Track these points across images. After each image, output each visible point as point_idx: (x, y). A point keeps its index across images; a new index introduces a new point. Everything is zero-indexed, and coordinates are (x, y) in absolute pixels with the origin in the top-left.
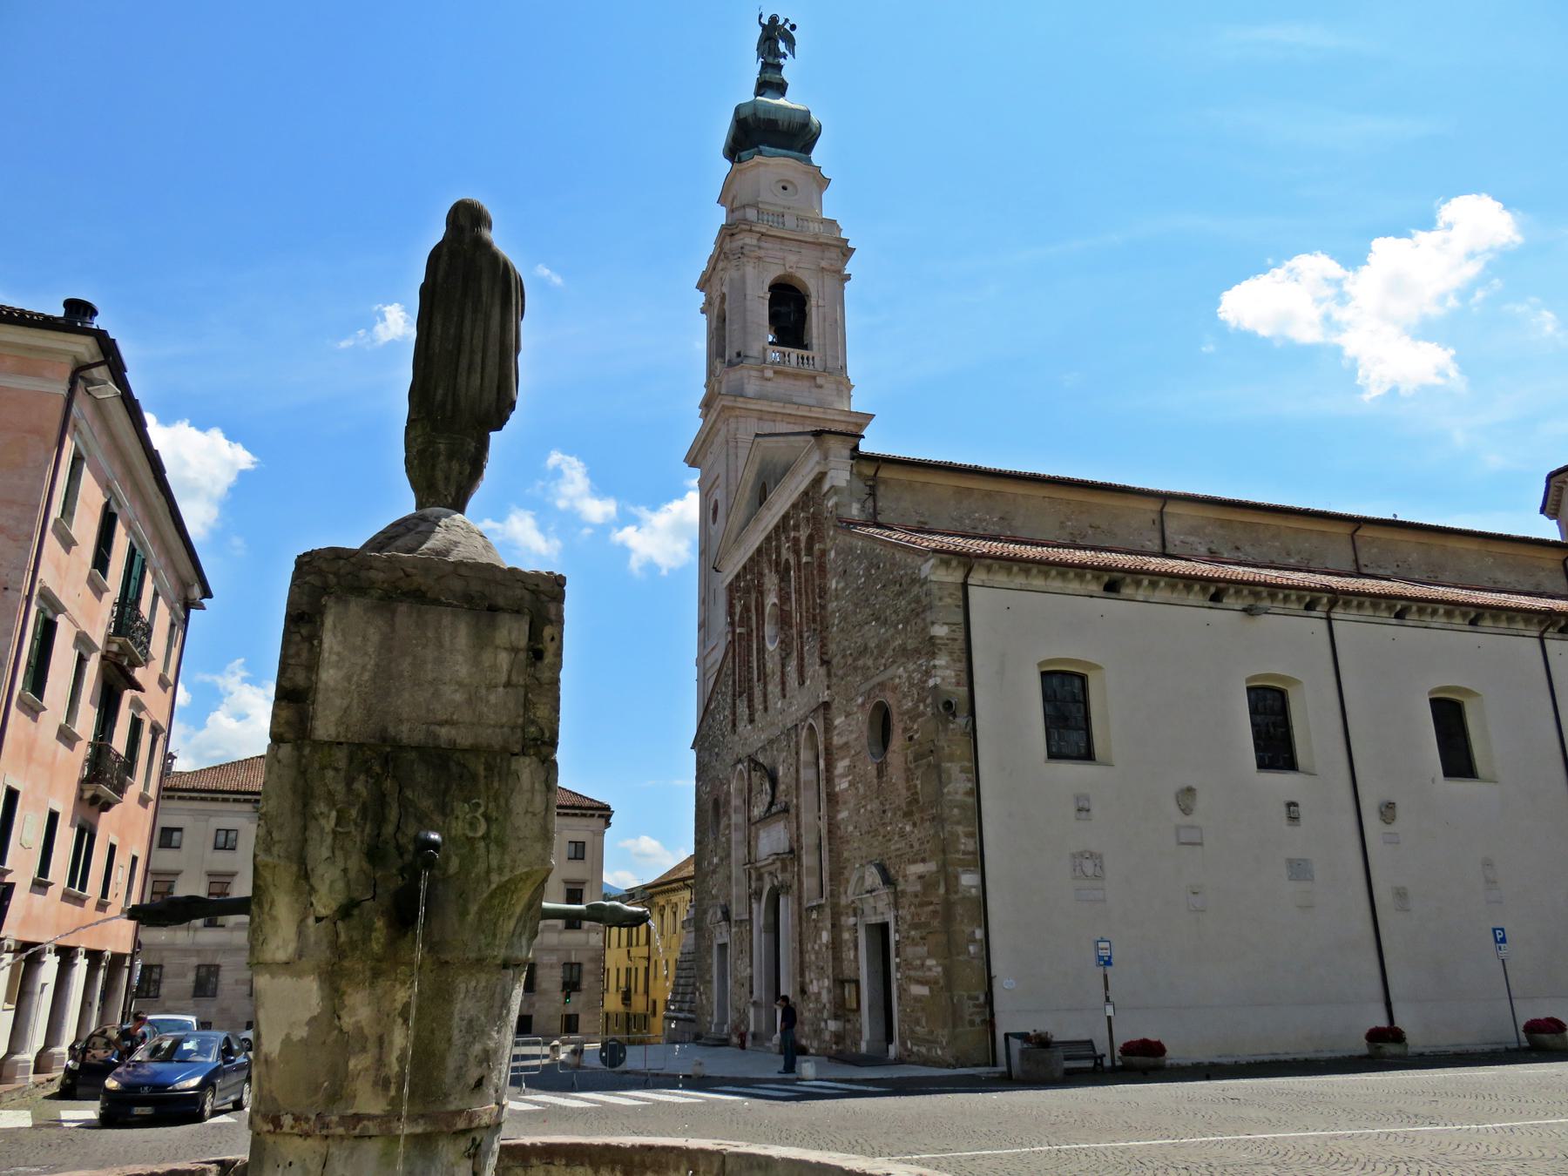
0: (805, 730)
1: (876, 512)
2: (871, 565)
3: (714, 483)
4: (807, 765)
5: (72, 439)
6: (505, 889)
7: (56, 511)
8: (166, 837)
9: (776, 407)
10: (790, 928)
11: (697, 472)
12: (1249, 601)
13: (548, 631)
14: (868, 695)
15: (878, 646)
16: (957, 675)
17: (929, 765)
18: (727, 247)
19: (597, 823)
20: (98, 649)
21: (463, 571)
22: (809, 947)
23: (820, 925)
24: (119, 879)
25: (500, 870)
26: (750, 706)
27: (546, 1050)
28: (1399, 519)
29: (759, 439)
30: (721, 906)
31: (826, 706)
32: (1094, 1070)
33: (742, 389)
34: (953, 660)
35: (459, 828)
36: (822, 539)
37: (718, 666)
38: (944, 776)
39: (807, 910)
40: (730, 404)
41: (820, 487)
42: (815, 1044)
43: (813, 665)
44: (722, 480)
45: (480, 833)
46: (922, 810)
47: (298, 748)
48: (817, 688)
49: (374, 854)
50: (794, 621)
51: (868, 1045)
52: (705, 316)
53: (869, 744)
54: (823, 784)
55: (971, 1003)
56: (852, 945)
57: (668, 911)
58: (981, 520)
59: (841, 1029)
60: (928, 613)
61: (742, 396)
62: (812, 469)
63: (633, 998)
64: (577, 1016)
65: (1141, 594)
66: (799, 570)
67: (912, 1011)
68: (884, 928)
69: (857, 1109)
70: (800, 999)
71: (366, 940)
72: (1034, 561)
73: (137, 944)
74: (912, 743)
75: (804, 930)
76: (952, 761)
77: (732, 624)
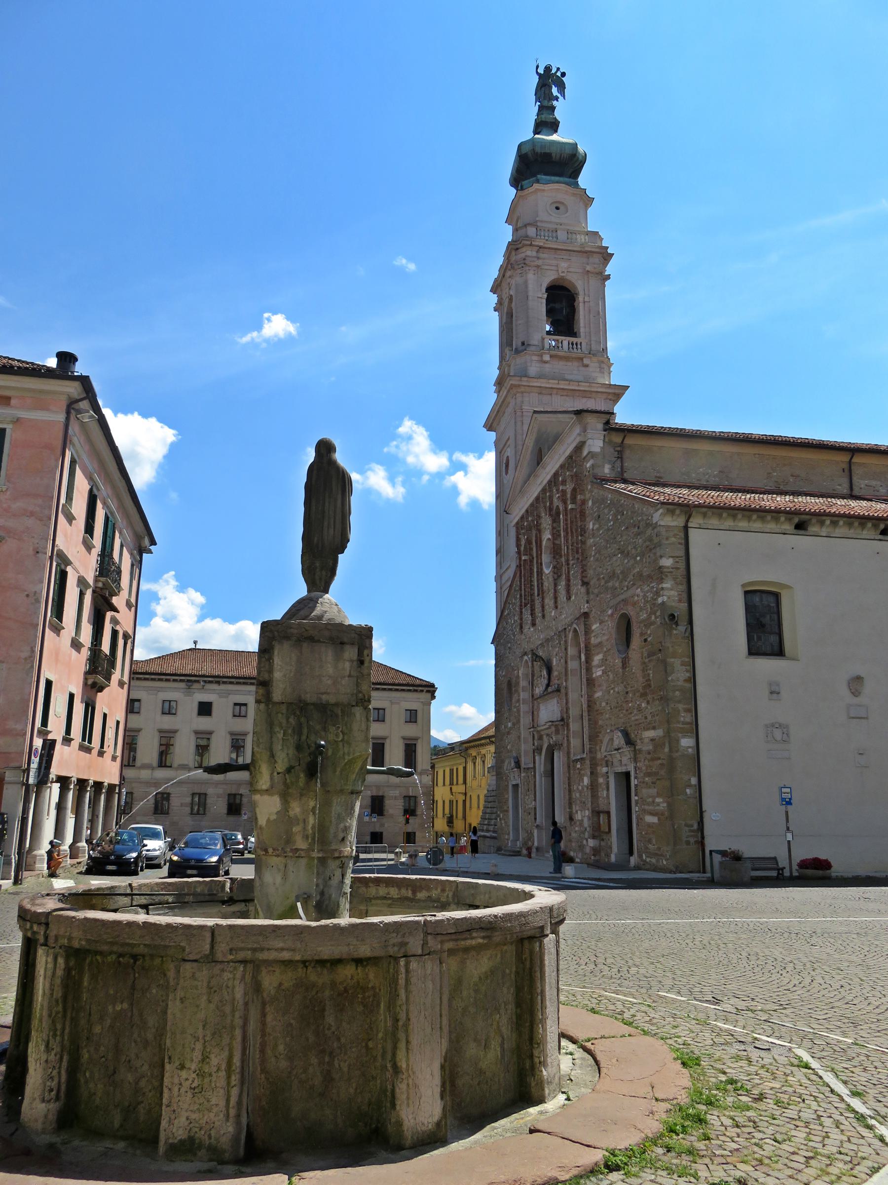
0: (571, 633)
1: (623, 471)
3: (505, 445)
5: (69, 450)
6: (351, 762)
7: (63, 500)
8: (132, 706)
9: (553, 384)
11: (493, 435)
13: (366, 652)
14: (615, 608)
15: (622, 572)
16: (679, 595)
18: (513, 258)
19: (425, 696)
20: (91, 586)
21: (329, 627)
23: (583, 772)
24: (110, 736)
25: (349, 754)
27: (392, 856)
29: (535, 415)
30: (514, 758)
31: (586, 615)
32: (777, 878)
34: (676, 583)
35: (331, 737)
36: (582, 492)
37: (509, 583)
38: (669, 668)
39: (573, 761)
40: (517, 383)
42: (580, 855)
43: (576, 585)
44: (511, 442)
45: (340, 739)
47: (267, 705)
48: (580, 602)
49: (299, 748)
52: (497, 313)
53: (616, 644)
54: (584, 671)
55: (687, 829)
57: (479, 760)
59: (598, 844)
60: (658, 549)
61: (526, 376)
62: (575, 439)
63: (455, 821)
64: (415, 833)
65: (824, 531)
66: (566, 515)
67: (646, 834)
68: (627, 775)
69: (596, 896)
70: (569, 823)
73: (122, 778)
75: (571, 775)
77: (519, 553)
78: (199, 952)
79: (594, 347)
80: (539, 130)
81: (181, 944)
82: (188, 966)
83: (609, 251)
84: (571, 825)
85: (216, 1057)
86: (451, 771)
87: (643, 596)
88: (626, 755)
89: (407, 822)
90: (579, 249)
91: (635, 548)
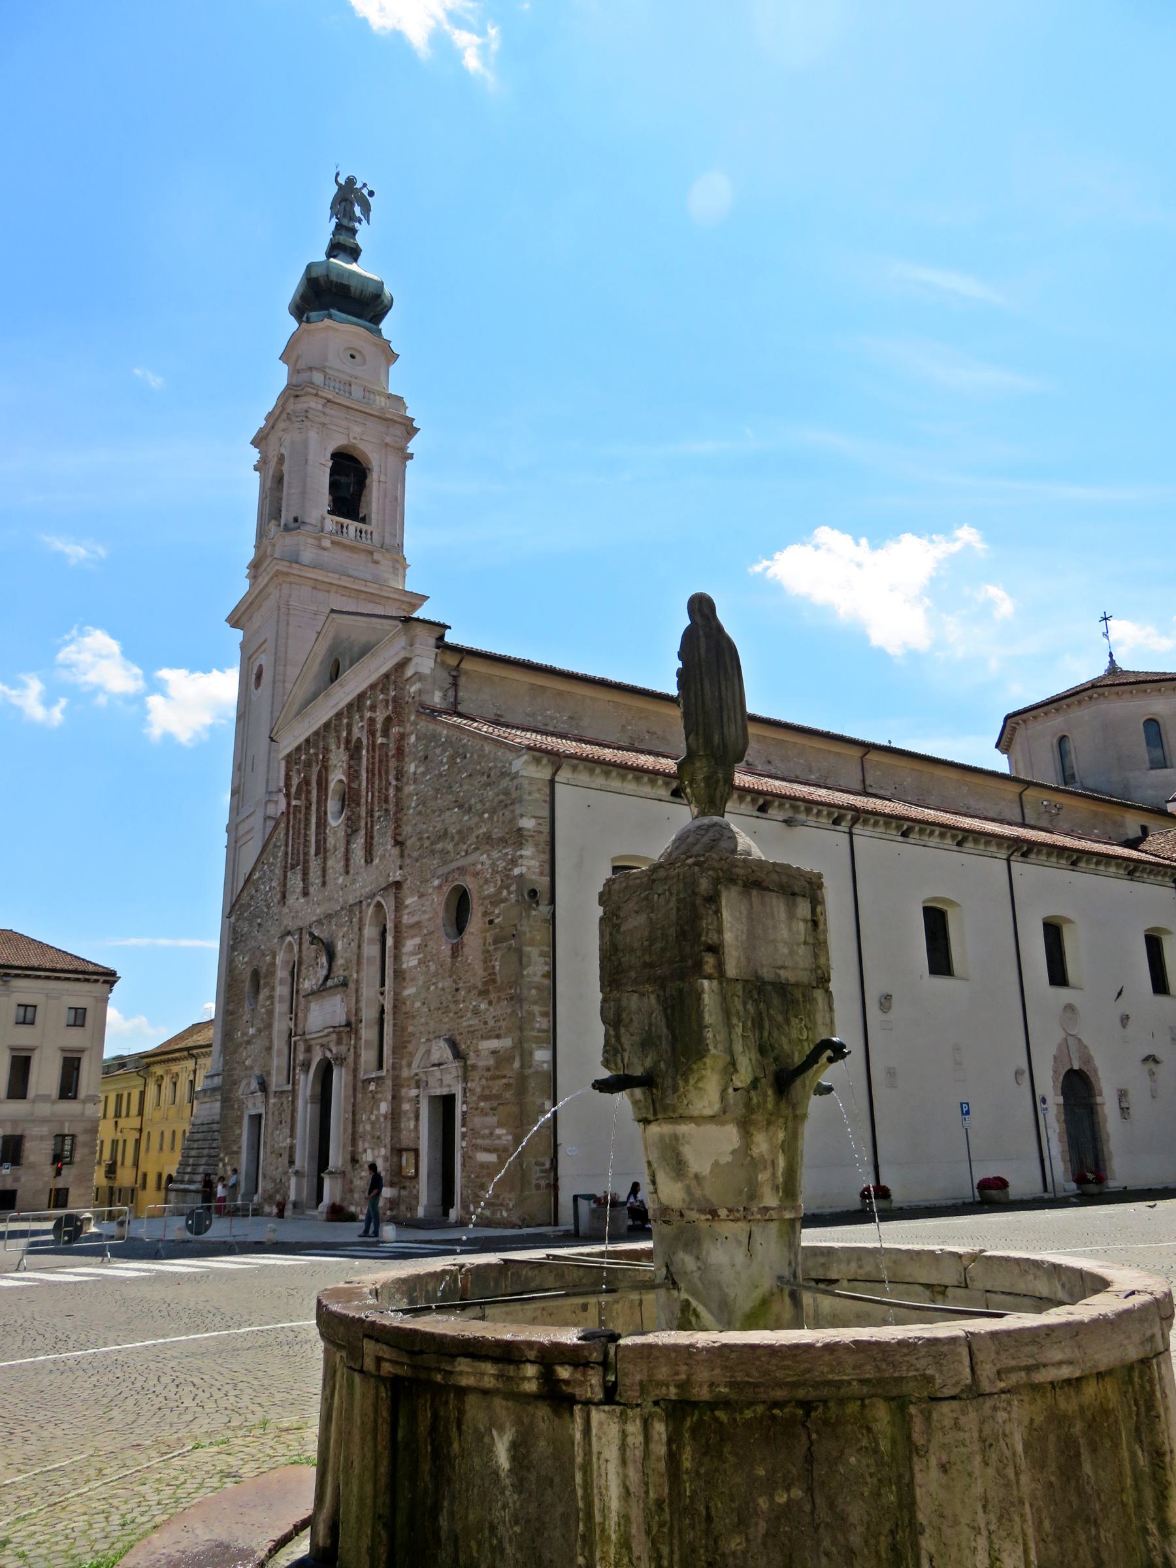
0: (372, 907)
1: (456, 702)
2: (456, 754)
3: (260, 647)
4: (371, 941)
9: (332, 578)
10: (342, 1099)
11: (238, 635)
12: (789, 814)
13: (819, 909)
14: (446, 878)
15: (459, 832)
17: (510, 948)
19: (98, 988)
21: (777, 869)
22: (364, 1117)
23: (379, 1096)
26: (305, 879)
28: (893, 745)
29: (334, 615)
30: (258, 1077)
31: (398, 885)
33: (298, 555)
36: (401, 723)
38: (525, 960)
39: (364, 1081)
40: (285, 570)
41: (403, 673)
46: (499, 990)
47: (721, 983)
50: (363, 800)
51: (425, 1211)
55: (538, 1168)
56: (412, 1115)
57: (167, 1083)
58: (552, 718)
59: (396, 1195)
60: (517, 806)
61: (297, 563)
64: (67, 1190)
66: (374, 750)
67: (477, 1177)
68: (448, 1102)
71: (765, 1102)
72: (614, 765)
74: (492, 926)
76: (533, 946)
78: (957, 1383)
79: (387, 540)
80: (335, 253)
81: (928, 1372)
82: (946, 1408)
83: (415, 424)
84: (354, 1169)
85: (1010, 1555)
86: (119, 1097)
87: (491, 865)
88: (450, 1073)
89: (58, 1173)
90: (376, 413)
91: (481, 801)
